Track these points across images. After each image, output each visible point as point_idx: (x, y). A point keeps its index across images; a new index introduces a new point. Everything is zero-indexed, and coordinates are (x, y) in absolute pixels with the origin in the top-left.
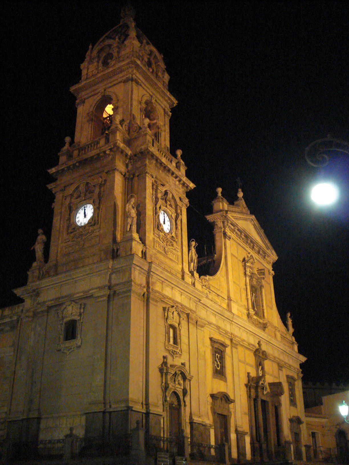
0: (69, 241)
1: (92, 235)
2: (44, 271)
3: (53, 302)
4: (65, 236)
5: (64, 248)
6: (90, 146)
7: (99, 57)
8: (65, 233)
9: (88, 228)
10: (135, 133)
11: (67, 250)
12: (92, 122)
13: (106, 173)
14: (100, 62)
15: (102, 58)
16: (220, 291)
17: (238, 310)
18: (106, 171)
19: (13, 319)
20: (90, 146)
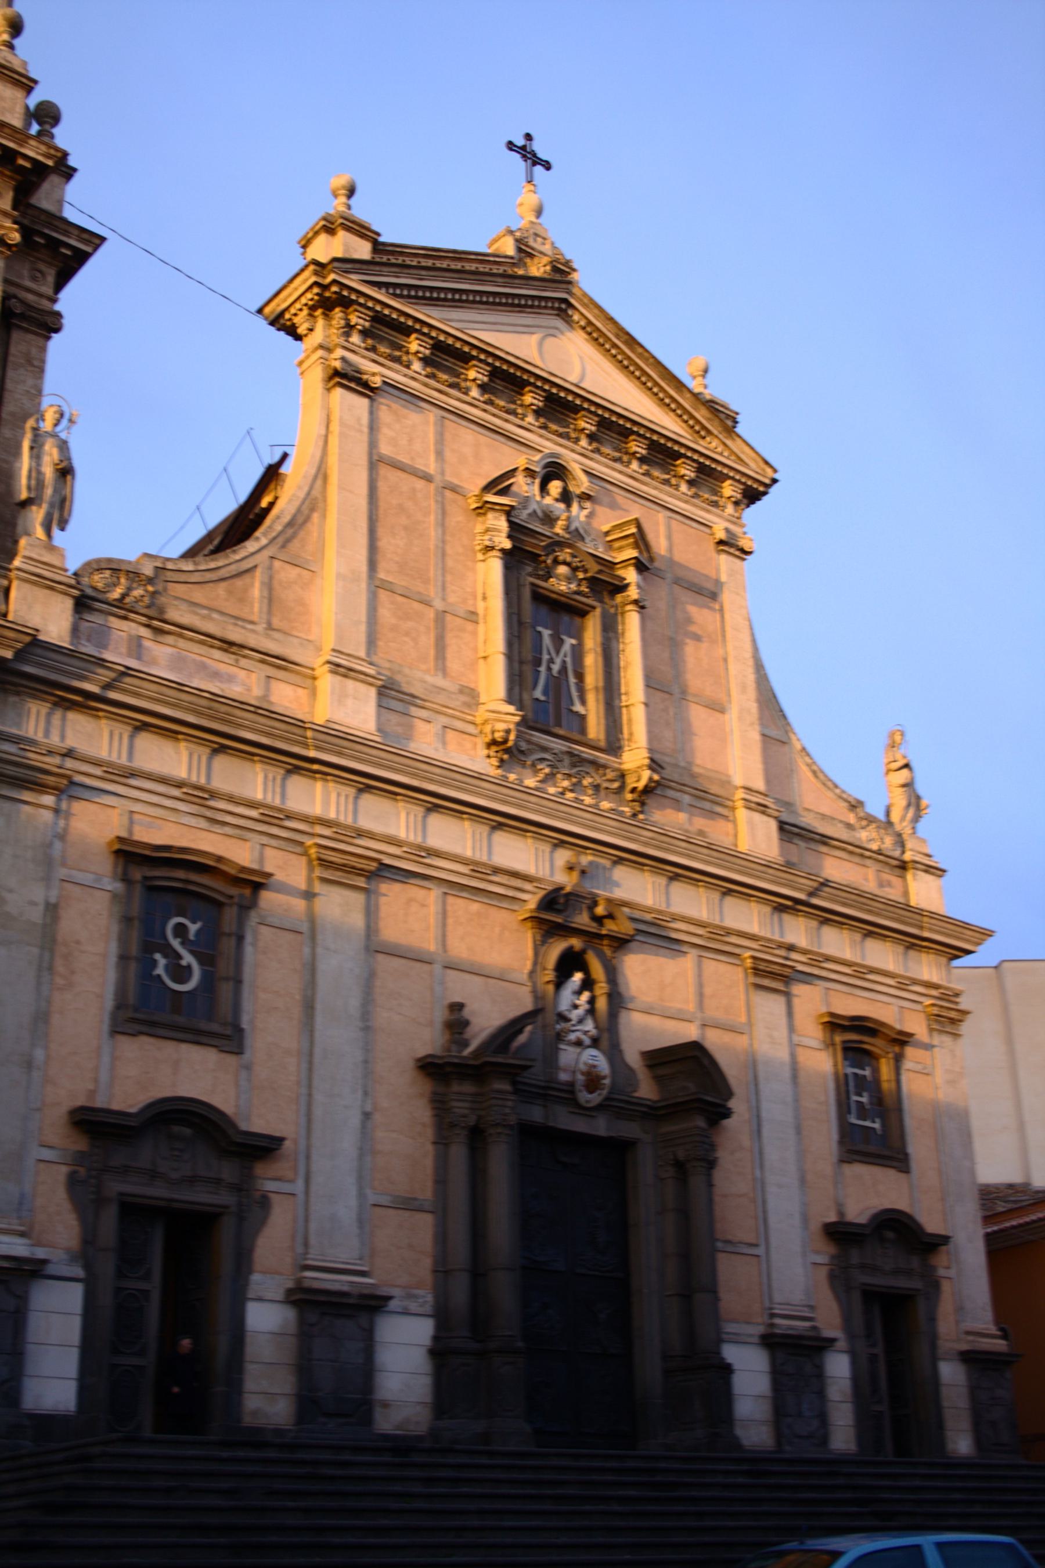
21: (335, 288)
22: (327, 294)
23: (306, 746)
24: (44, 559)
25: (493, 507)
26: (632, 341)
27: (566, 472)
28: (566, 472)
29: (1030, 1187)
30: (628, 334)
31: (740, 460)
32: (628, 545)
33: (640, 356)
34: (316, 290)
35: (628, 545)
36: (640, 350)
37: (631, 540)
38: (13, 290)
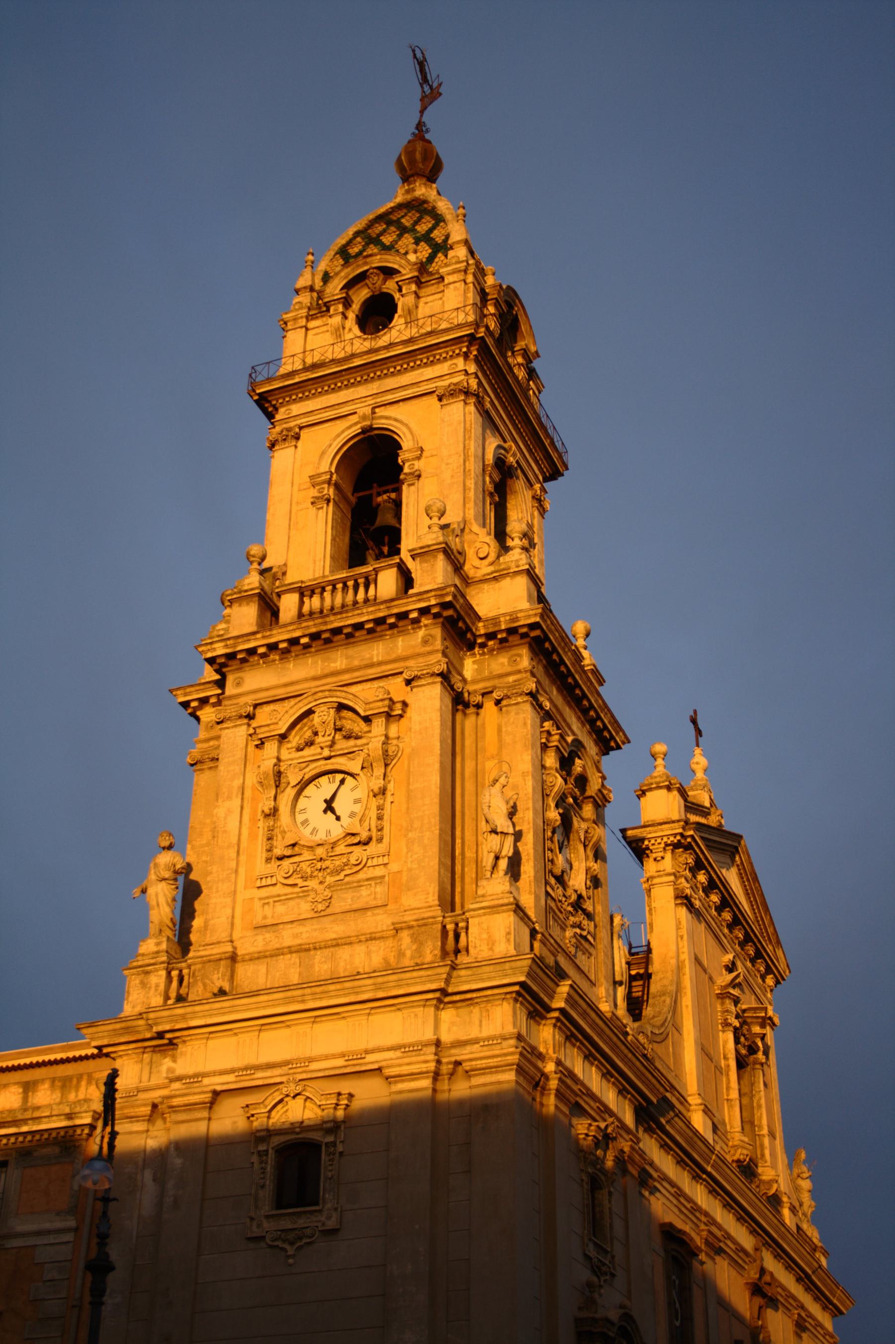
0: (275, 885)
1: (361, 876)
2: (185, 972)
3: (231, 1078)
4: (261, 867)
5: (257, 904)
6: (339, 586)
7: (347, 303)
8: (261, 854)
9: (341, 848)
10: (486, 562)
11: (268, 911)
12: (328, 504)
13: (408, 682)
14: (351, 316)
15: (356, 306)
16: (673, 1074)
17: (556, 1106)
18: (406, 675)
19: (78, 1122)
20: (339, 586)
21: (689, 840)
22: (683, 841)
23: (834, 1296)
24: (467, 811)
25: (728, 995)
26: (756, 879)
27: (583, 750)
28: (583, 750)
29: (163, 1149)
30: (756, 874)
31: (777, 960)
32: (757, 1022)
33: (756, 888)
34: (678, 837)
35: (757, 1022)
36: (757, 885)
37: (760, 1020)
38: (413, 553)
